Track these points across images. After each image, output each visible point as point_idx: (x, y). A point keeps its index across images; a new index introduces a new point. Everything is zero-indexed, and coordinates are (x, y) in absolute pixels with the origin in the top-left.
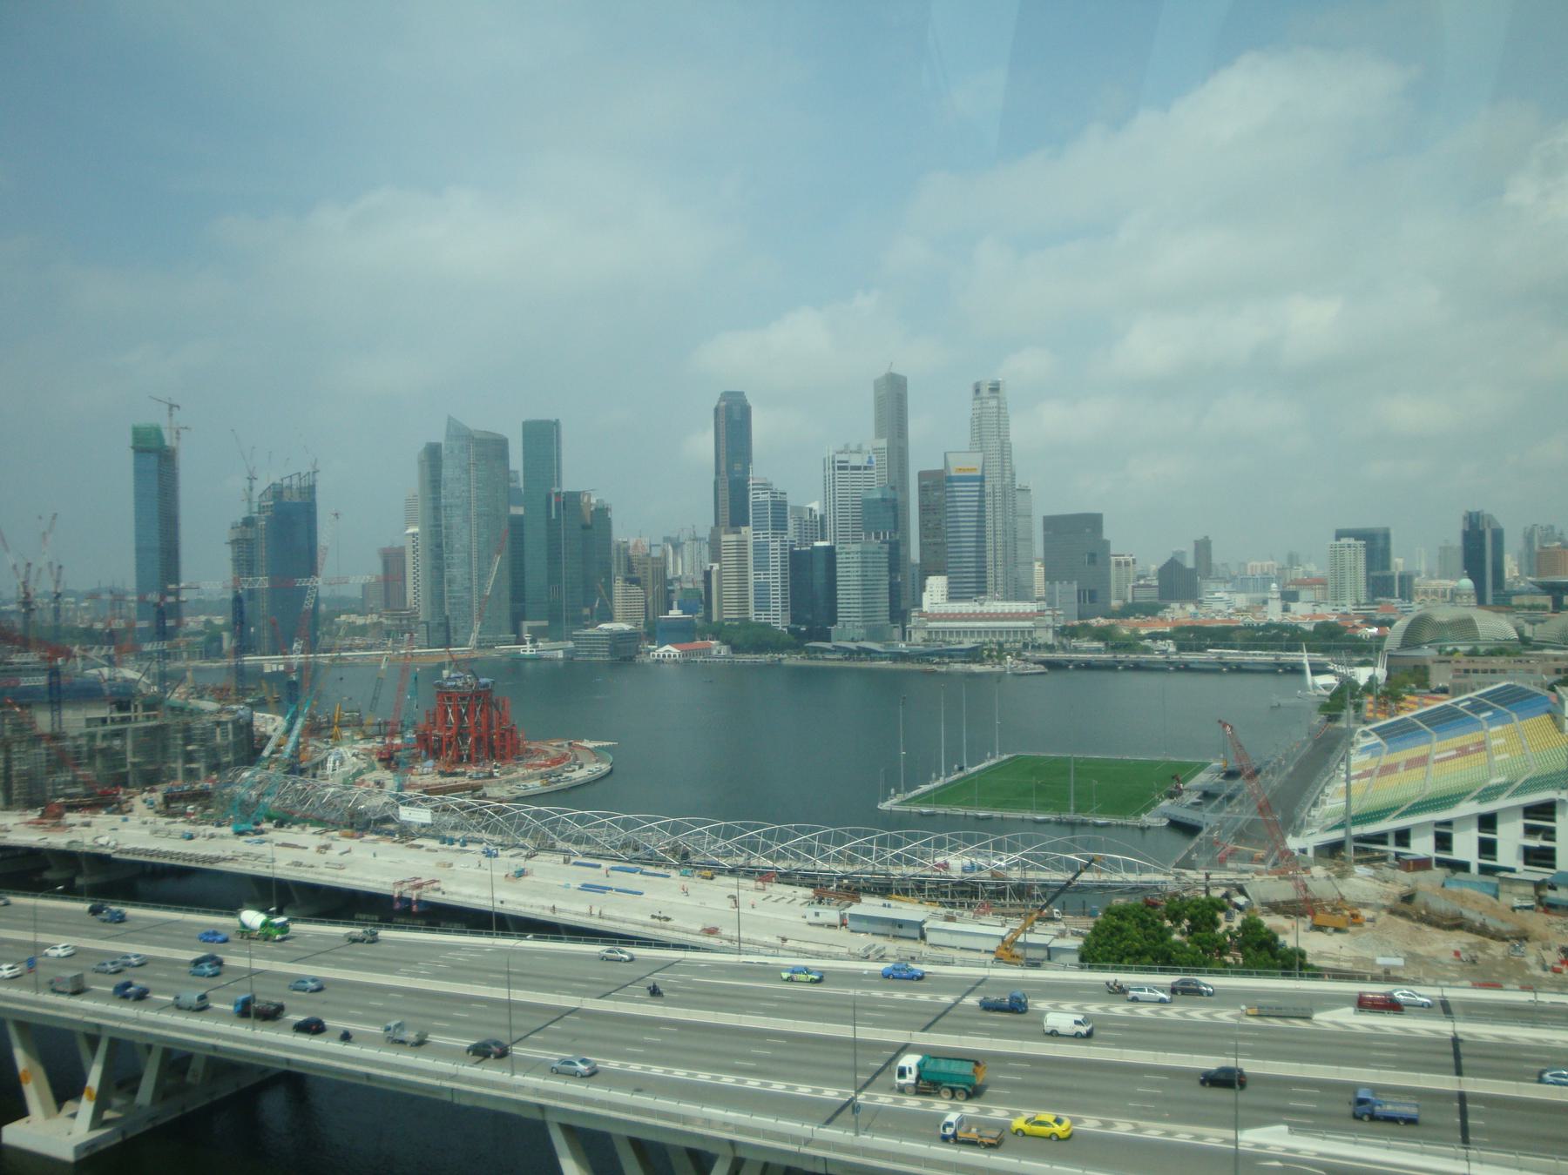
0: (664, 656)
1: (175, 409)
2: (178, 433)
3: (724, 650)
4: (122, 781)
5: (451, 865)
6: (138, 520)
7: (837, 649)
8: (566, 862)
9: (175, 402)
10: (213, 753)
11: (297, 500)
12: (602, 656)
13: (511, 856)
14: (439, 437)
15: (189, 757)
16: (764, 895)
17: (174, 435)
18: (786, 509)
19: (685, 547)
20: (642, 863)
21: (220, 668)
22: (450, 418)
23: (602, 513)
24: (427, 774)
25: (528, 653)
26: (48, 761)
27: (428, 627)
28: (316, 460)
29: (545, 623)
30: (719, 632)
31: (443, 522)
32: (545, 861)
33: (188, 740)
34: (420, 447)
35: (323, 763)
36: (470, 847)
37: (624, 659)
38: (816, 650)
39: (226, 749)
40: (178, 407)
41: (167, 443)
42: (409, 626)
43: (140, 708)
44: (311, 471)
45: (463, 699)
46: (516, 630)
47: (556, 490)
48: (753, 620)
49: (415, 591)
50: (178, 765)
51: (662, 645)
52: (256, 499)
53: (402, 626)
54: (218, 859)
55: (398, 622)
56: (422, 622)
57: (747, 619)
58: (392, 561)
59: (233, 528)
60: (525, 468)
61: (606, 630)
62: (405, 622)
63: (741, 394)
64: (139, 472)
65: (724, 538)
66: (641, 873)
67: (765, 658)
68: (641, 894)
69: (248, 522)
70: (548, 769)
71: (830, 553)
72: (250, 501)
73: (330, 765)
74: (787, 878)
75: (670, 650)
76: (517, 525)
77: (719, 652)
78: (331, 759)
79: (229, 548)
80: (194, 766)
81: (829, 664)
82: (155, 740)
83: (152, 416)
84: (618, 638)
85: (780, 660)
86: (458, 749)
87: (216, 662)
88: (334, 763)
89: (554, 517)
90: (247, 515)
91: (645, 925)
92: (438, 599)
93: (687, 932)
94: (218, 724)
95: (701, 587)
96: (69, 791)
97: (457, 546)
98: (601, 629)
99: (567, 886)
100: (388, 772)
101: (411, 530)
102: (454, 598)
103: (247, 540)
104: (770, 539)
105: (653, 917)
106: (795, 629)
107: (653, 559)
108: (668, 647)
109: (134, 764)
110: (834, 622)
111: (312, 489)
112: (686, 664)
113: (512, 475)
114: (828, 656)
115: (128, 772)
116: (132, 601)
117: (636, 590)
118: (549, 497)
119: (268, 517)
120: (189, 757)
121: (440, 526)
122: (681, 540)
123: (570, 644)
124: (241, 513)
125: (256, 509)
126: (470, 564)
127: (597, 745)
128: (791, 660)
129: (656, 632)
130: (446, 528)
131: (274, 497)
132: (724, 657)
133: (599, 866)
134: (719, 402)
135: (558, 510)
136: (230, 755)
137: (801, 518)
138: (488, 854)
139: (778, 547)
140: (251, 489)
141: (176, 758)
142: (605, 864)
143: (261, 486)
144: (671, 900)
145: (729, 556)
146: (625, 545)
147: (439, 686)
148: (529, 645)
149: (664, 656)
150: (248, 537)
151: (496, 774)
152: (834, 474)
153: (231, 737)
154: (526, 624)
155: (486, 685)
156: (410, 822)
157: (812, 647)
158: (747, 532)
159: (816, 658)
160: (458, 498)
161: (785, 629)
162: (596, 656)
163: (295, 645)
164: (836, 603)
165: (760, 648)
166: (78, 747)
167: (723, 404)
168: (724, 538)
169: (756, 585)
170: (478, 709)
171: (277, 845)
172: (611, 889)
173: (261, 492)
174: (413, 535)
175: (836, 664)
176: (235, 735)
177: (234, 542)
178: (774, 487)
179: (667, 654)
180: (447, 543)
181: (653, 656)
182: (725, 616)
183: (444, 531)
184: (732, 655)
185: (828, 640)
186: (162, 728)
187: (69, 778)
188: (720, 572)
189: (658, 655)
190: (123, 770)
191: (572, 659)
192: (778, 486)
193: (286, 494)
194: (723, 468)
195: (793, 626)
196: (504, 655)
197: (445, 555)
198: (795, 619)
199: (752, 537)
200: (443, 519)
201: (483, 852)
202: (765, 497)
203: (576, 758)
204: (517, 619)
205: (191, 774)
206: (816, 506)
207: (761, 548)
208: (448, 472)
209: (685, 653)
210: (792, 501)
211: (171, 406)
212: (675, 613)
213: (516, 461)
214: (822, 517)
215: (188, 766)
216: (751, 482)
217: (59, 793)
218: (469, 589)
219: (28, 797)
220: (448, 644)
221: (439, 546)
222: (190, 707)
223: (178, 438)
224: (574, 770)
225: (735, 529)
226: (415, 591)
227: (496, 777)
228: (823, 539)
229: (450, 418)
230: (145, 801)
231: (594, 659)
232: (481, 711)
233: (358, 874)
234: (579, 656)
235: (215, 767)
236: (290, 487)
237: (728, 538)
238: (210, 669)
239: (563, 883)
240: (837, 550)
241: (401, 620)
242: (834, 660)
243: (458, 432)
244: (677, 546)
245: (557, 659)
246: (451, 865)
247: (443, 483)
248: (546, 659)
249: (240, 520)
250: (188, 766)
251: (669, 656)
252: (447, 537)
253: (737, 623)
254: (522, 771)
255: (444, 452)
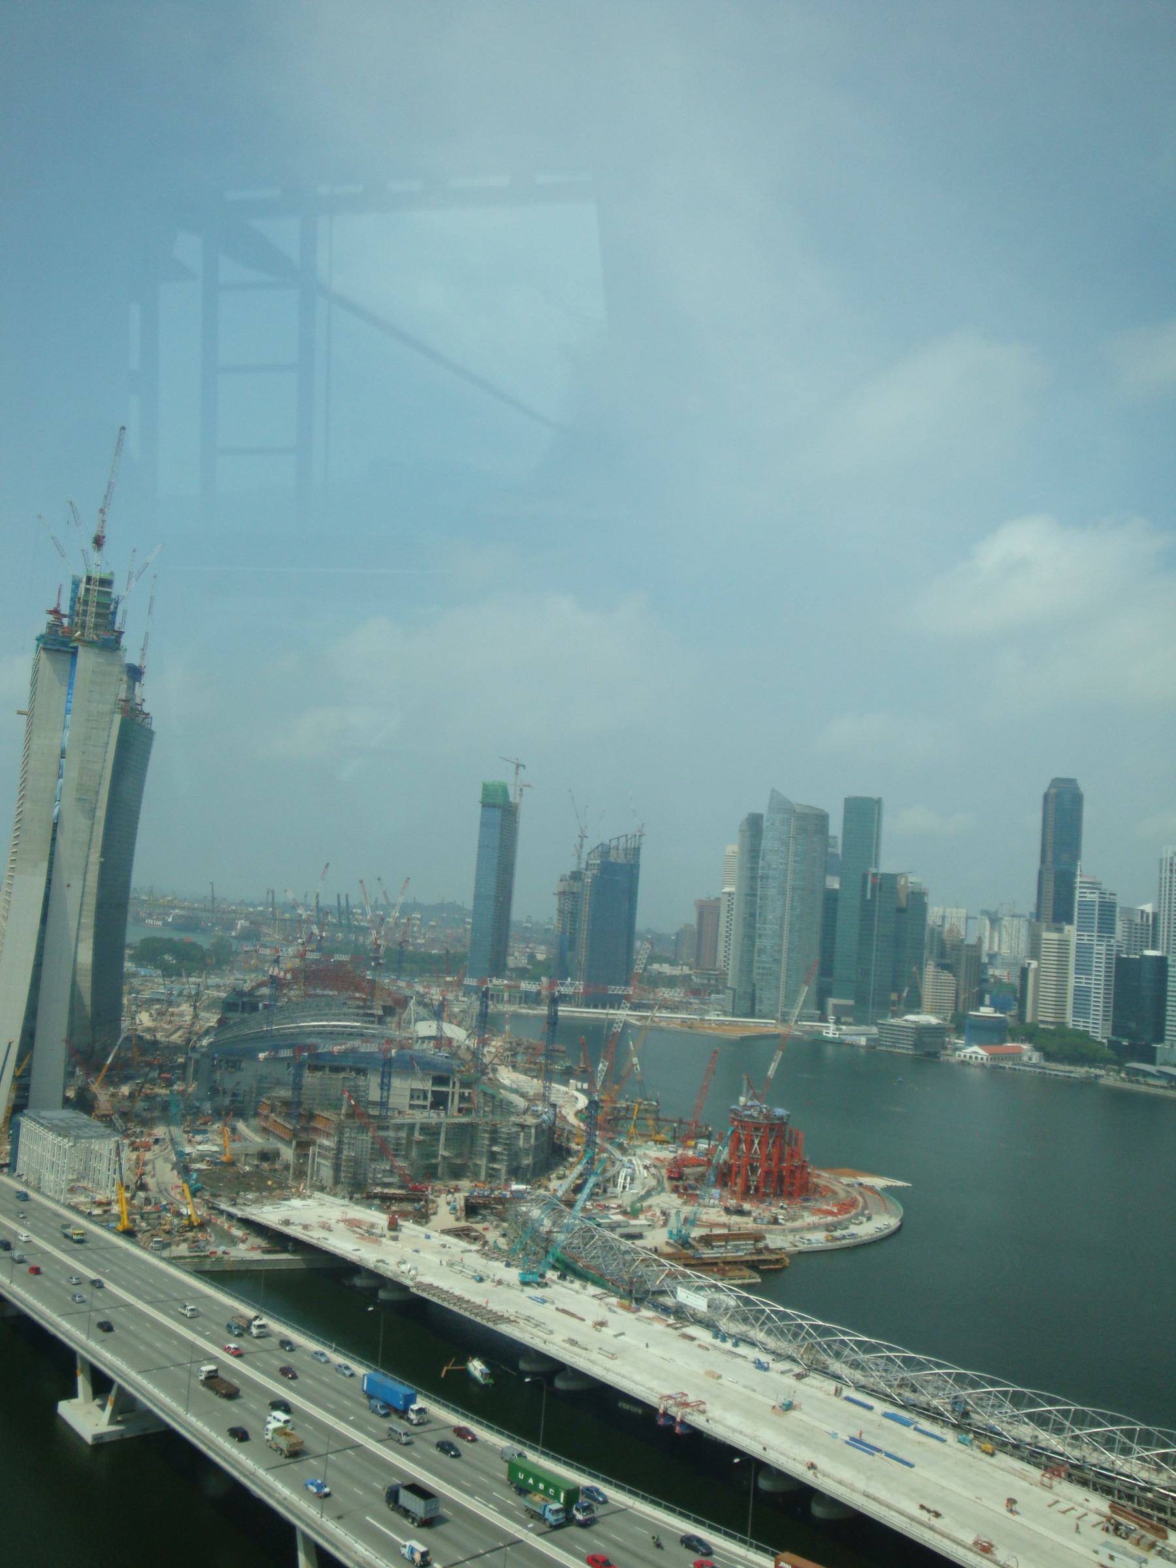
0: (971, 1057)
1: (521, 768)
2: (521, 790)
3: (1036, 1057)
4: (431, 1173)
5: (720, 1377)
6: (479, 868)
7: (1162, 1075)
8: (838, 1392)
9: (521, 762)
10: (514, 1155)
11: (621, 860)
12: (906, 1048)
13: (783, 1373)
14: (762, 808)
15: (493, 1157)
16: (1049, 1497)
17: (518, 792)
18: (1115, 911)
19: (1004, 923)
20: (919, 1414)
21: (535, 1016)
22: (773, 790)
23: (918, 900)
24: (713, 1207)
25: (830, 1035)
26: (372, 1148)
27: (734, 995)
28: (643, 824)
29: (851, 1002)
30: (1031, 1034)
31: (759, 893)
32: (817, 1386)
33: (494, 1141)
34: (743, 816)
35: (615, 1177)
36: (743, 1349)
37: (929, 1054)
38: (1137, 1072)
39: (527, 1152)
40: (524, 766)
41: (511, 799)
42: (716, 986)
43: (457, 1085)
44: (638, 834)
45: (757, 1129)
46: (821, 1006)
47: (873, 870)
48: (1070, 1026)
49: (728, 955)
50: (483, 1162)
51: (969, 1043)
52: (584, 856)
53: (710, 985)
54: (501, 1318)
55: (706, 982)
56: (729, 988)
57: (1063, 1023)
58: (707, 911)
59: (561, 880)
60: (844, 837)
61: (913, 1022)
62: (713, 982)
63: (1072, 781)
64: (484, 824)
65: (1046, 935)
66: (916, 1429)
67: (1080, 1072)
68: (911, 1466)
69: (576, 876)
70: (835, 1219)
71: (1161, 962)
72: (579, 857)
73: (621, 1181)
74: (1078, 1475)
75: (976, 1052)
76: (831, 898)
77: (1030, 1059)
78: (622, 1174)
79: (555, 899)
80: (495, 1166)
81: (1152, 1091)
82: (463, 1135)
83: (501, 775)
84: (923, 1031)
85: (1097, 1077)
86: (747, 1180)
87: (534, 1009)
88: (625, 1179)
89: (869, 897)
90: (575, 869)
91: (912, 1519)
92: (747, 967)
93: (954, 1541)
94: (523, 1127)
95: (1016, 982)
96: (386, 1180)
97: (770, 917)
98: (906, 1021)
99: (834, 1435)
100: (674, 1196)
101: (727, 889)
102: (763, 968)
103: (573, 893)
104: (1095, 943)
105: (922, 1507)
106: (1116, 1042)
107: (968, 946)
108: (976, 1048)
109: (444, 1157)
110: (1160, 1038)
111: (636, 851)
112: (993, 1071)
113: (830, 840)
114: (1151, 1081)
115: (438, 1164)
116: (469, 923)
117: (947, 976)
118: (865, 877)
119: (593, 875)
120: (493, 1157)
121: (755, 895)
122: (1000, 916)
123: (874, 1030)
124: (570, 866)
125: (583, 865)
126: (781, 937)
127: (889, 1183)
128: (1110, 1078)
129: (963, 1026)
130: (761, 899)
131: (601, 856)
132: (1034, 1066)
133: (870, 1408)
134: (1049, 788)
135: (873, 890)
136: (531, 1158)
137: (1130, 921)
138: (760, 1366)
139: (1104, 952)
140: (581, 846)
141: (482, 1156)
142: (880, 1407)
143: (590, 844)
144: (944, 1483)
145: (1049, 955)
146: (939, 929)
147: (735, 1112)
148: (832, 1026)
149: (971, 1057)
150: (575, 891)
151: (780, 1221)
152: (1171, 878)
153: (533, 1141)
154: (832, 1002)
155: (781, 1118)
156: (686, 1305)
157: (1133, 1068)
158: (1071, 931)
159: (1138, 1082)
160: (775, 869)
161: (1105, 1041)
162: (899, 1048)
163: (601, 1066)
164: (1167, 976)
165: (1078, 1059)
166: (398, 1139)
167: (1053, 791)
168: (1046, 935)
169: (1077, 989)
170: (771, 1141)
171: (557, 1309)
172: (879, 1451)
173: (589, 851)
174: (729, 894)
175: (1160, 1092)
176: (536, 1139)
177: (562, 894)
178: (1104, 886)
179: (974, 1056)
180: (760, 914)
181: (959, 1056)
182: (1041, 1018)
183: (758, 901)
184: (1043, 1064)
185: (1151, 1060)
186: (473, 1126)
187: (388, 1168)
188: (1037, 970)
189: (965, 1056)
190: (433, 1161)
191: (874, 1048)
192: (1107, 886)
193: (613, 853)
194: (1049, 857)
195: (1114, 1038)
196: (806, 1032)
197: (758, 926)
198: (1118, 1029)
199: (1076, 937)
200: (759, 889)
201: (755, 1363)
202: (1093, 897)
203: (865, 1207)
204: (823, 994)
205: (492, 1175)
206: (1148, 908)
207: (1084, 951)
208: (769, 842)
209: (994, 1056)
210: (1121, 902)
211: (518, 766)
212: (986, 1011)
213: (836, 828)
214: (1155, 916)
215: (491, 1165)
216: (1078, 879)
217: (378, 1181)
218: (777, 961)
219: (352, 1181)
220: (752, 1014)
221: (753, 915)
222: (501, 1097)
223: (521, 795)
224: (861, 1223)
225: (1057, 925)
226: (728, 955)
227: (781, 1224)
228: (1154, 948)
229: (773, 790)
230: (448, 1204)
231: (898, 1050)
232: (774, 1143)
233: (626, 1370)
234: (883, 1045)
235: (516, 1173)
236: (617, 848)
237: (1049, 936)
238: (527, 1016)
239: (830, 1429)
240: (1170, 962)
241: (709, 979)
242: (1157, 1086)
243: (780, 804)
244: (995, 921)
245: (859, 1046)
246: (720, 1377)
247: (761, 854)
248: (848, 1044)
249: (569, 873)
250: (491, 1165)
251: (976, 1058)
252: (761, 907)
253: (1052, 1027)
254: (809, 1219)
255: (765, 824)
